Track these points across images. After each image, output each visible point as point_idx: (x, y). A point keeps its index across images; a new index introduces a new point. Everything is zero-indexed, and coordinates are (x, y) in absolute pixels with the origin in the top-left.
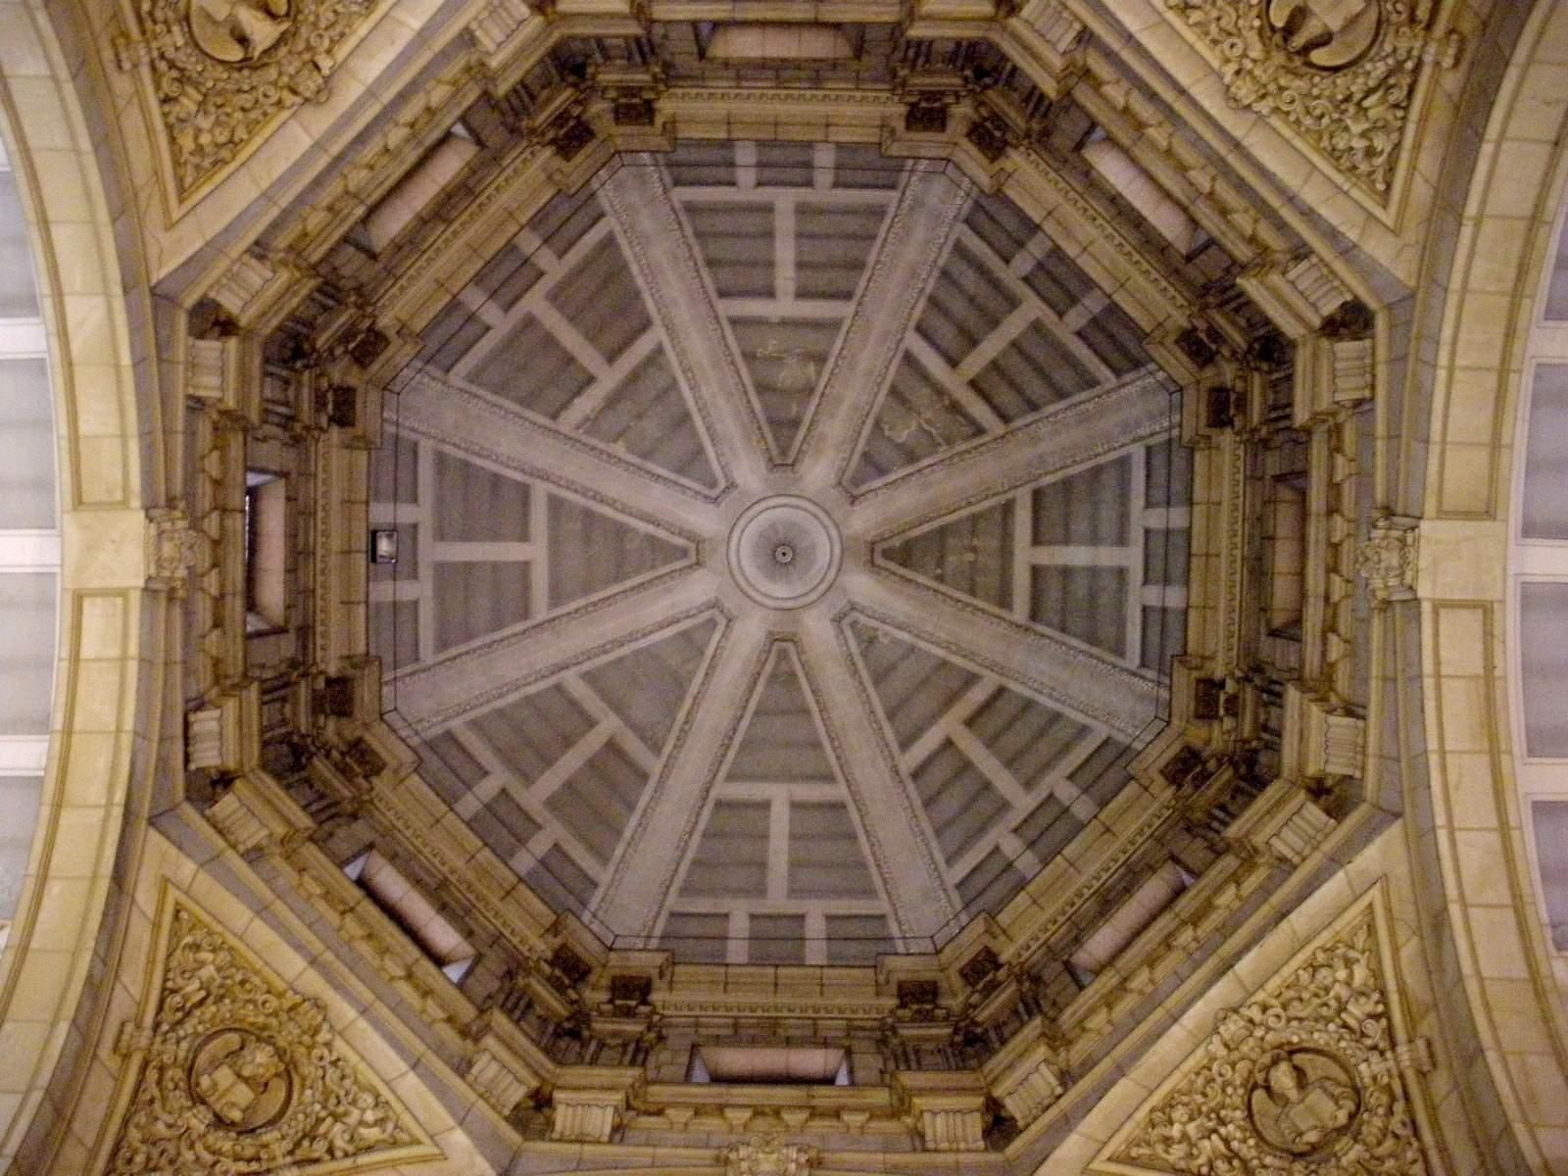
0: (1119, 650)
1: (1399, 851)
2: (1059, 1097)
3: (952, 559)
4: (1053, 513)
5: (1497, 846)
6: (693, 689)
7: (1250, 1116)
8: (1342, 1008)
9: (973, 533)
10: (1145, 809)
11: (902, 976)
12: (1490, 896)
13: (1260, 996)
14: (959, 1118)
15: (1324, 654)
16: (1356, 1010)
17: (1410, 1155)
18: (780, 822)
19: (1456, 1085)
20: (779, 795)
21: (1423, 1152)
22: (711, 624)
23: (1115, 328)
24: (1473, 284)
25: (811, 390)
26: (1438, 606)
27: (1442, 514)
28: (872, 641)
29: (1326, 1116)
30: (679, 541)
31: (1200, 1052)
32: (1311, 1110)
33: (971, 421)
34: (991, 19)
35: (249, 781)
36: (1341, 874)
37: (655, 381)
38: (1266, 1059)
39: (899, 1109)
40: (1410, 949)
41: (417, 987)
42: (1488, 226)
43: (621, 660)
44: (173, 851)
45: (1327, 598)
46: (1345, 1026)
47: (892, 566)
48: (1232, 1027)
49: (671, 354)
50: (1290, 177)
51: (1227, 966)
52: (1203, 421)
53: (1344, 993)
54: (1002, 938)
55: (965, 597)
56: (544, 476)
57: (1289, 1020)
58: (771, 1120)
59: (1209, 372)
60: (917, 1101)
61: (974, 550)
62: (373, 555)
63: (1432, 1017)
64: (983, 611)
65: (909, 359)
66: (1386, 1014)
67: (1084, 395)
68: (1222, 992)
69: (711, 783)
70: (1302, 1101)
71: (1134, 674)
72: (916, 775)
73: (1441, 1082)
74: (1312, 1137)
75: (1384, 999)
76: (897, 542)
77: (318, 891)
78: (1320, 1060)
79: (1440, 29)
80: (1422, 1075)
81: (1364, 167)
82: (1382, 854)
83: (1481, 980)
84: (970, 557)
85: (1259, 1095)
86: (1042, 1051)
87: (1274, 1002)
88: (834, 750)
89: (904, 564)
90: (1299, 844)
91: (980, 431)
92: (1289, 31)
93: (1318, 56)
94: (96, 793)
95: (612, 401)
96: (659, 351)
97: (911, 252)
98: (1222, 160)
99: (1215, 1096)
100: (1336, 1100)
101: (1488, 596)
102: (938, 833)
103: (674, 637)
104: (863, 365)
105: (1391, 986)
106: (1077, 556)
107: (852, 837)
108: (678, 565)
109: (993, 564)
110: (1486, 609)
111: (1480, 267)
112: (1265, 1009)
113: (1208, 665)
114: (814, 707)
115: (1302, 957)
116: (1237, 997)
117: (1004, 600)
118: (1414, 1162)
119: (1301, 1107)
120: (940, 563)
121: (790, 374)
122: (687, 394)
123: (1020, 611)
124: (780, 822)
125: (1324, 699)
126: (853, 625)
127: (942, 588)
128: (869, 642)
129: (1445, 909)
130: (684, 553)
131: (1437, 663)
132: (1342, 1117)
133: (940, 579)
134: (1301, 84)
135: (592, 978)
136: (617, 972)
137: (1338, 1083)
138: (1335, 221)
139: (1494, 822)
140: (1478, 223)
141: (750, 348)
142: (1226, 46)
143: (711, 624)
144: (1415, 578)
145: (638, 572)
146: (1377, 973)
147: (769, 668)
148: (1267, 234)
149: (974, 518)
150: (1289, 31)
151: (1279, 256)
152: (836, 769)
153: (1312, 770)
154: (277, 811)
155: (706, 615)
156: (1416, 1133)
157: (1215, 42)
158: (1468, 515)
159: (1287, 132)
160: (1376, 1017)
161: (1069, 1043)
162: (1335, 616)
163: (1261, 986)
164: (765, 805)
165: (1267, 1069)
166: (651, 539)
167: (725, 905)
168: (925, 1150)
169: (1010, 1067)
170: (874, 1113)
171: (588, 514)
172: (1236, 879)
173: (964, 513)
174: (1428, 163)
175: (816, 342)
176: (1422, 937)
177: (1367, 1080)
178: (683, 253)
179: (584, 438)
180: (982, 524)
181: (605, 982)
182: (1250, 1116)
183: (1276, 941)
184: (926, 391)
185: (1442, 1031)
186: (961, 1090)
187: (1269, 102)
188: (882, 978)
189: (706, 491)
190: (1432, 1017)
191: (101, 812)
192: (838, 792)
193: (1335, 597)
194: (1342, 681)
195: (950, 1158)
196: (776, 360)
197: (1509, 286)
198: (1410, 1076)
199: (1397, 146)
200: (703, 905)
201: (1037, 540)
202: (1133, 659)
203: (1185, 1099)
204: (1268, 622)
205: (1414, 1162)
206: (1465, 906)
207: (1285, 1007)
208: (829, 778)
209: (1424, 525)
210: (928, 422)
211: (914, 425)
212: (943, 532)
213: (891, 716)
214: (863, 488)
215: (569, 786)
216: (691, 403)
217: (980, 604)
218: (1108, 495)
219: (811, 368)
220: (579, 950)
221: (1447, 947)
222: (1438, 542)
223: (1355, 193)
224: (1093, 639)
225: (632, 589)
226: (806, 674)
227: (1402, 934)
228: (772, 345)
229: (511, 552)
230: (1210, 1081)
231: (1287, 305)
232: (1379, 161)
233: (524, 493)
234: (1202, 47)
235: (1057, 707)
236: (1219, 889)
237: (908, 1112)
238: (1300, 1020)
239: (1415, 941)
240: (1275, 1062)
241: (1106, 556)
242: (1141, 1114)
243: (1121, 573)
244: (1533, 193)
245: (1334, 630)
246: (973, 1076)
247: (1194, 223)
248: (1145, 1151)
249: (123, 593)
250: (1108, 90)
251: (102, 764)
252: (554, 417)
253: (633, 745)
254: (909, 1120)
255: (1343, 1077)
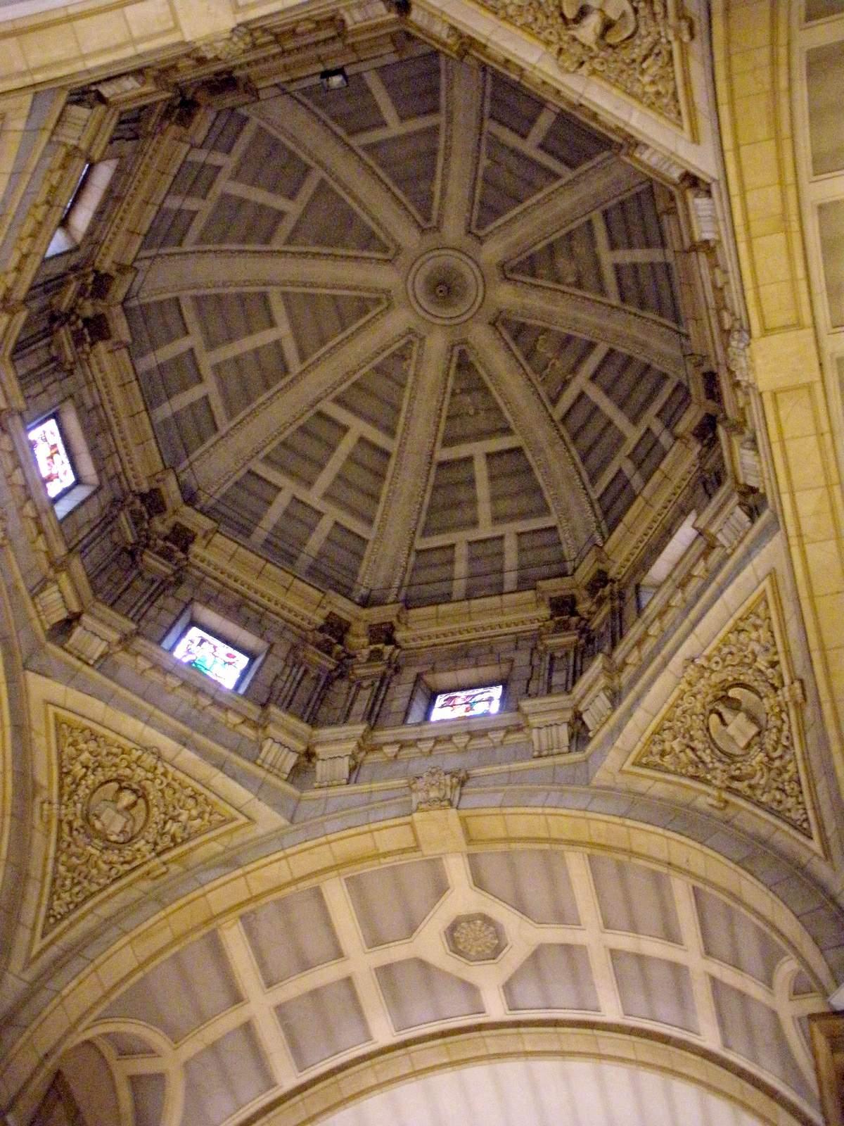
0: (427, 532)
1: (276, 826)
2: (88, 664)
3: (468, 399)
4: (508, 464)
5: (284, 880)
6: (340, 251)
7: (102, 784)
8: (174, 819)
9: (488, 410)
10: (306, 608)
11: (164, 490)
12: (253, 884)
13: (171, 769)
14: (62, 604)
15: (386, 744)
16: (172, 827)
17: (102, 881)
18: (264, 338)
19: (147, 894)
20: (283, 330)
21: (105, 887)
22: (385, 249)
23: (624, 497)
24: (592, 823)
25: (558, 281)
26: (410, 824)
27: (463, 820)
28: (403, 358)
29: (112, 829)
30: (435, 214)
31: (131, 745)
32: (113, 820)
33: (559, 394)
34: (737, 482)
35: (107, 112)
36: (251, 796)
37: (539, 179)
38: (135, 786)
39: (58, 566)
40: (216, 847)
41: (20, 262)
42: (624, 829)
43: (343, 200)
44: (26, 112)
45: (420, 740)
46: (165, 823)
47: (455, 359)
48: (149, 760)
49: (556, 185)
50: (648, 701)
51: (184, 742)
52: (553, 595)
53: (183, 818)
54: (204, 542)
55: (444, 414)
56: (450, 121)
57: (161, 791)
58: (23, 497)
59: (585, 593)
60: (64, 575)
61: (476, 413)
62: (326, 74)
63: (181, 869)
64: (437, 430)
65: (591, 346)
66: (176, 845)
67: (584, 474)
68: (167, 745)
69: (277, 285)
70: (118, 811)
71: (410, 548)
72: (320, 414)
73: (146, 885)
74: (98, 825)
75: (184, 841)
76: (472, 358)
77: (54, 183)
78: (143, 814)
79: (725, 795)
80: (148, 873)
81: (656, 749)
82: (269, 818)
83: (204, 895)
84: (472, 412)
85: (115, 785)
86: (115, 637)
87: (170, 777)
88: (323, 355)
89: (459, 366)
90: (270, 759)
91: (554, 401)
92: (725, 699)
93: (714, 718)
94: (36, 58)
95: (514, 152)
96: (557, 177)
97: (655, 343)
98: (659, 653)
99: (107, 761)
100: (122, 832)
101: (424, 847)
102: (284, 444)
103: (368, 228)
104: (582, 316)
105: (192, 844)
106: (483, 490)
107: (267, 387)
108: (418, 217)
109: (469, 429)
110: (417, 848)
111: (602, 826)
112: (165, 774)
113: (403, 628)
114: (349, 332)
115: (198, 787)
116: (168, 754)
117: (448, 442)
118: (98, 884)
119: (113, 813)
120: (463, 391)
121: (565, 266)
122: (533, 200)
123: (444, 454)
124: (264, 338)
125: (360, 748)
126: (410, 342)
127: (448, 396)
128: (401, 356)
129: (240, 866)
130: (426, 217)
131: (378, 830)
132: (113, 838)
133: (453, 394)
134: (699, 709)
135: (100, 302)
136: (108, 316)
137: (132, 828)
138: (626, 730)
139: (297, 875)
140: (623, 825)
141: (573, 238)
142: (717, 659)
143: (385, 249)
144: (423, 810)
145: (406, 193)
146: (199, 833)
147: (366, 295)
148: (629, 671)
149: (498, 409)
150: (725, 699)
151: (616, 681)
152: (310, 361)
153: (318, 750)
154: (94, 139)
155: (391, 245)
156: (114, 880)
157: (719, 650)
158: (466, 831)
159: (671, 700)
160: (173, 838)
161: (125, 650)
162: (411, 746)
163: (177, 769)
164: (272, 324)
165: (129, 788)
166: (431, 197)
167: (194, 327)
168: (33, 598)
169: (102, 621)
170: (48, 553)
171: (434, 153)
172: (246, 721)
173: (500, 401)
174: (659, 789)
175: (588, 280)
176: (224, 853)
177: (137, 846)
178: (624, 187)
179: (484, 141)
180: (493, 416)
181: (100, 310)
182: (102, 784)
183: (205, 770)
184: (572, 361)
185: (174, 878)
186: (79, 596)
187: (687, 688)
188: (159, 476)
189: (474, 223)
190: (181, 869)
191: (24, 68)
192: (295, 367)
193: (420, 745)
194: (374, 757)
195: (33, 613)
196: (571, 255)
197: (595, 840)
198: (145, 868)
199: (667, 771)
200: (189, 315)
201: (489, 456)
202: (421, 544)
203: (102, 744)
204: (426, 672)
205: (98, 884)
206: (244, 875)
207: (168, 785)
208: (303, 357)
209: (453, 811)
210: (554, 365)
211: (550, 355)
212: (485, 390)
213: (356, 385)
214: (501, 329)
215: (242, 202)
216: (528, 203)
217: (442, 427)
218: (524, 503)
219: (571, 279)
220: (113, 288)
221: (219, 871)
222: (447, 819)
223: (640, 745)
224: (432, 509)
225: (393, 194)
226: (369, 321)
227: (225, 840)
228: (580, 250)
229: (389, 112)
230: (116, 755)
231: (590, 687)
232: (657, 759)
233: (435, 110)
234: (715, 642)
235: (383, 499)
236: (237, 712)
237: (57, 572)
238: (163, 797)
239: (220, 848)
240: (134, 791)
241: (484, 510)
242: (86, 722)
243: (474, 523)
244: (644, 851)
245: (401, 747)
246: (91, 597)
247: (658, 587)
248: (67, 733)
249: (177, 28)
250: (702, 563)
251: (57, 53)
252: (492, 117)
253: (286, 227)
254: (51, 574)
255: (137, 828)
